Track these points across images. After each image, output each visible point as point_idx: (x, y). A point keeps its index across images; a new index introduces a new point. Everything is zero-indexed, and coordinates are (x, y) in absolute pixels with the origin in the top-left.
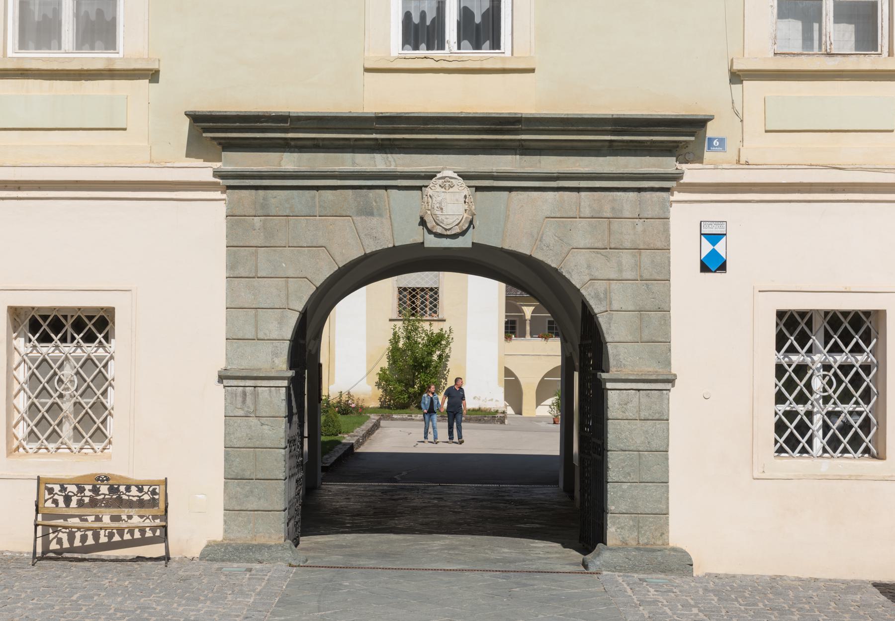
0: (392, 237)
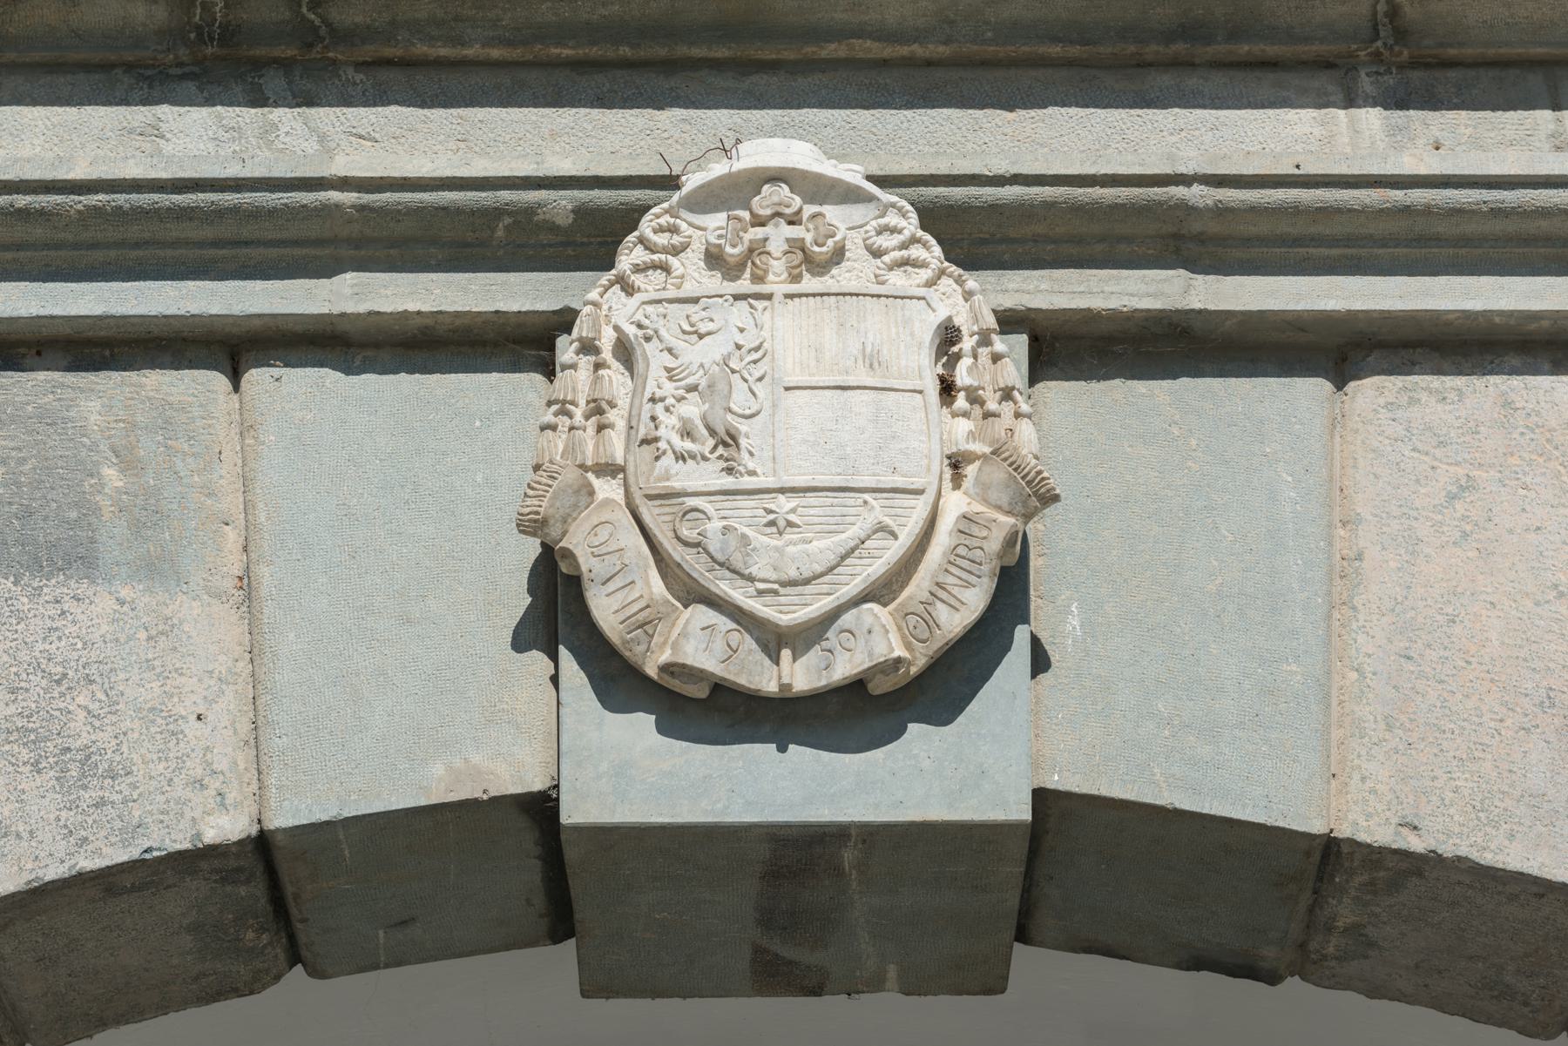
0: (244, 759)
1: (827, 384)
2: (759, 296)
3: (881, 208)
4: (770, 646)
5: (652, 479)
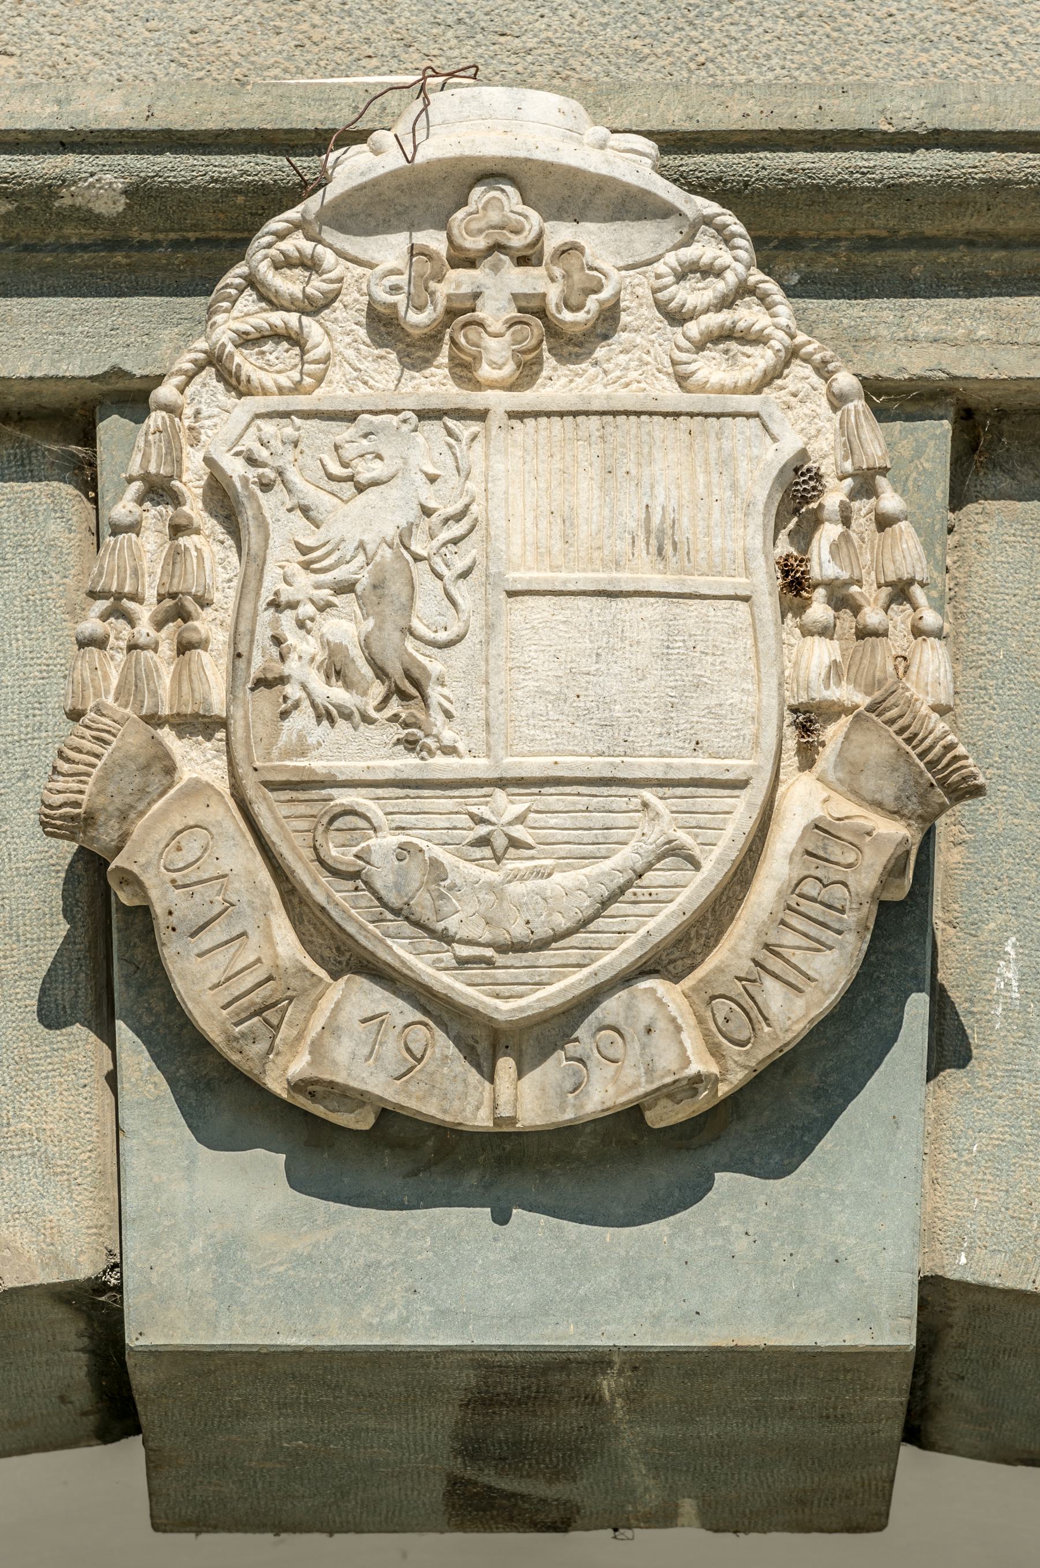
1: (581, 587)
2: (462, 414)
3: (685, 230)
4: (479, 1049)
5: (275, 752)
